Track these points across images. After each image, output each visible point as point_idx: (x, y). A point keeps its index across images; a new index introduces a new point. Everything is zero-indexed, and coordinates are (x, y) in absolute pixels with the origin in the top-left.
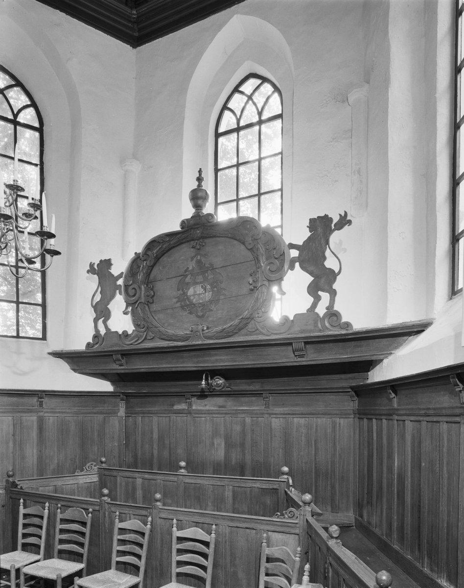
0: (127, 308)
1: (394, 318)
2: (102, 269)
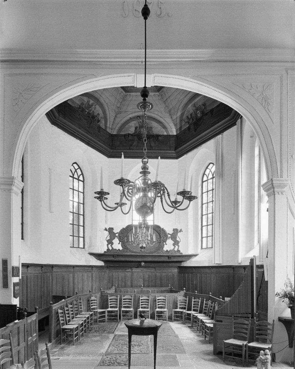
0: (119, 242)
1: (190, 253)
2: (110, 230)
